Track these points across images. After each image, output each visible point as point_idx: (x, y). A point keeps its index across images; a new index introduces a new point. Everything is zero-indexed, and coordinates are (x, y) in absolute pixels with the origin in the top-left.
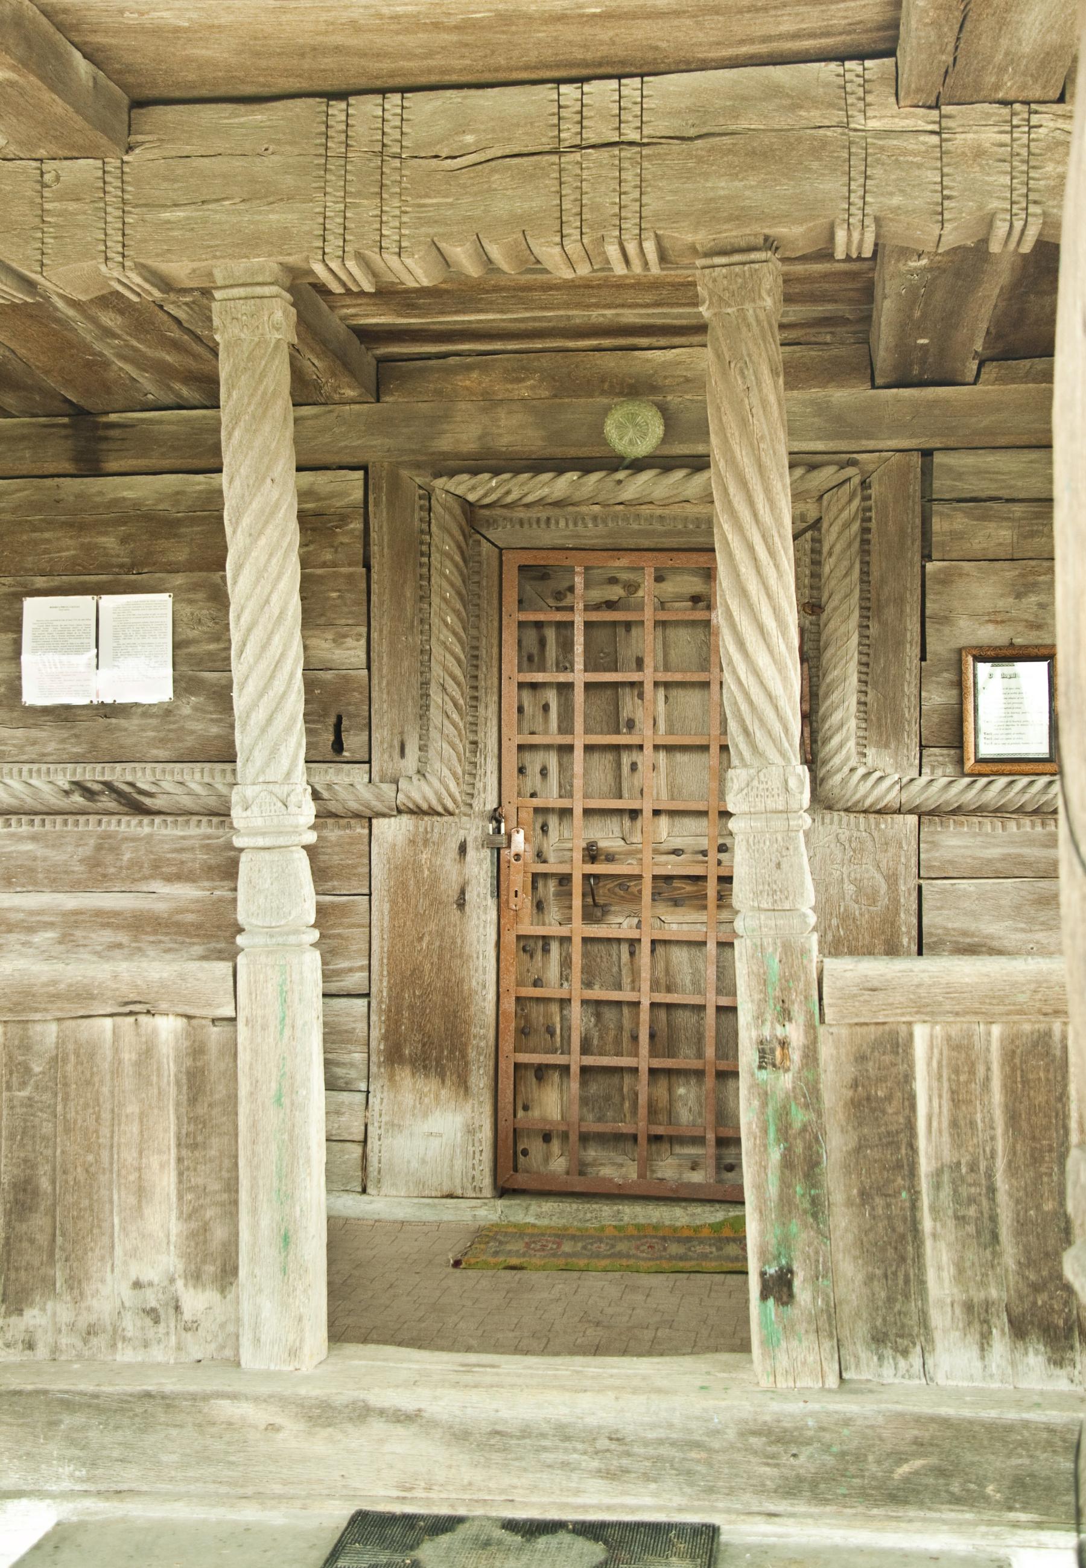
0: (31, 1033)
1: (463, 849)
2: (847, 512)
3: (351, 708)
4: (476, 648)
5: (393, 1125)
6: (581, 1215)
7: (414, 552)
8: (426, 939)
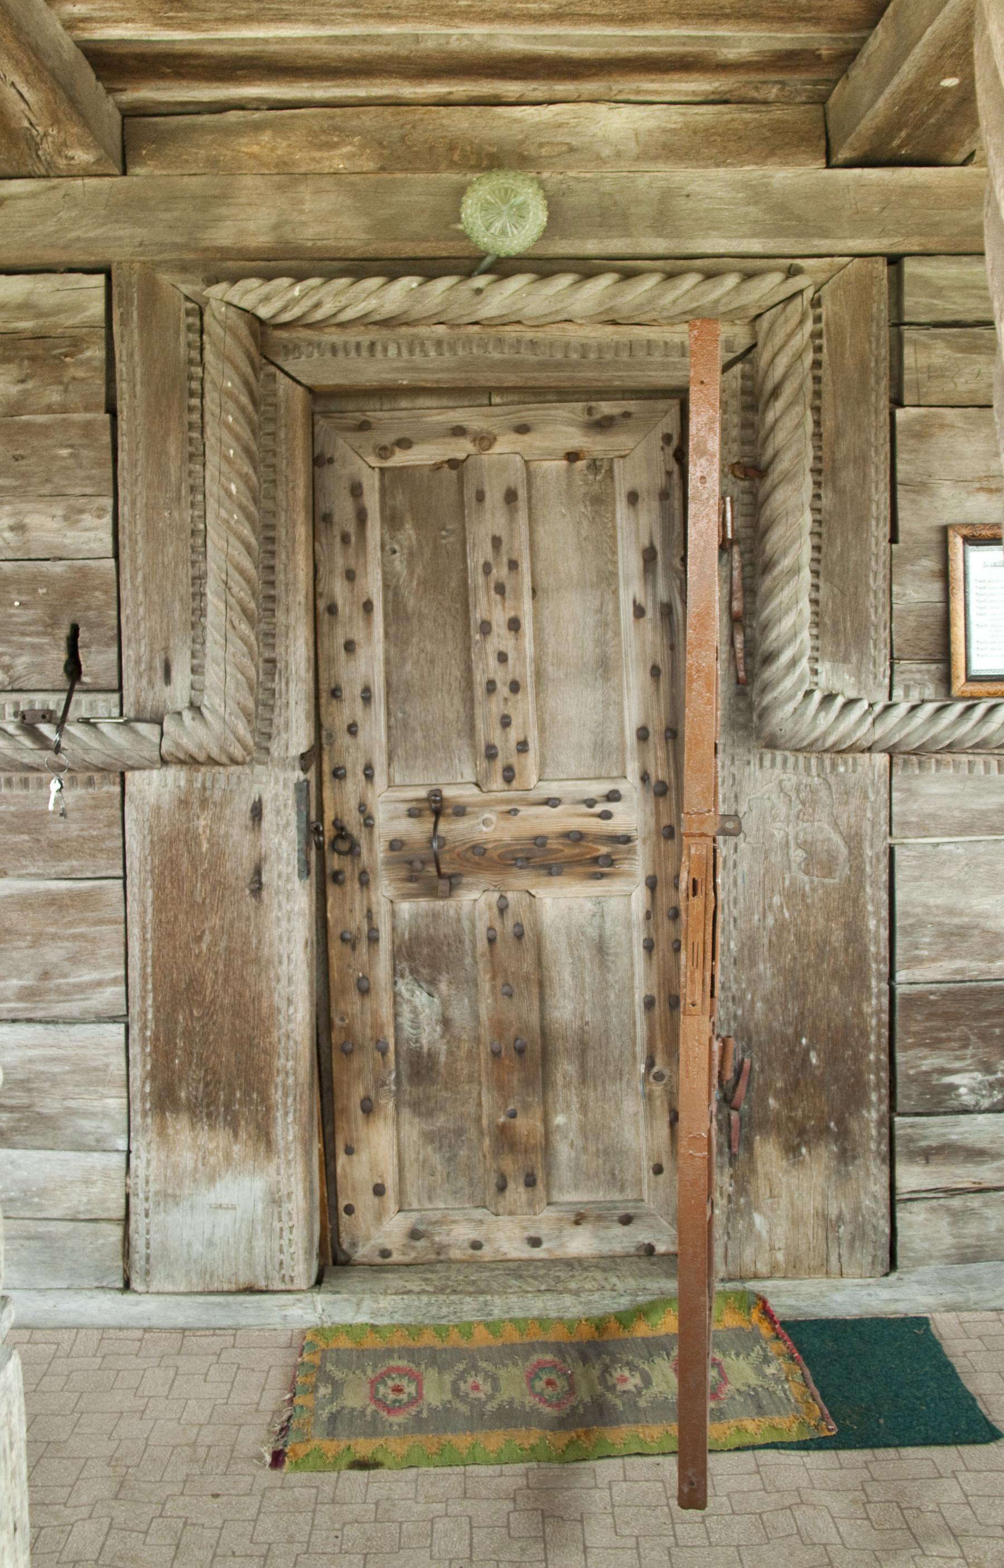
1: (257, 812)
2: (798, 337)
3: (91, 614)
4: (271, 527)
5: (166, 1196)
6: (434, 1310)
7: (180, 390)
8: (207, 938)
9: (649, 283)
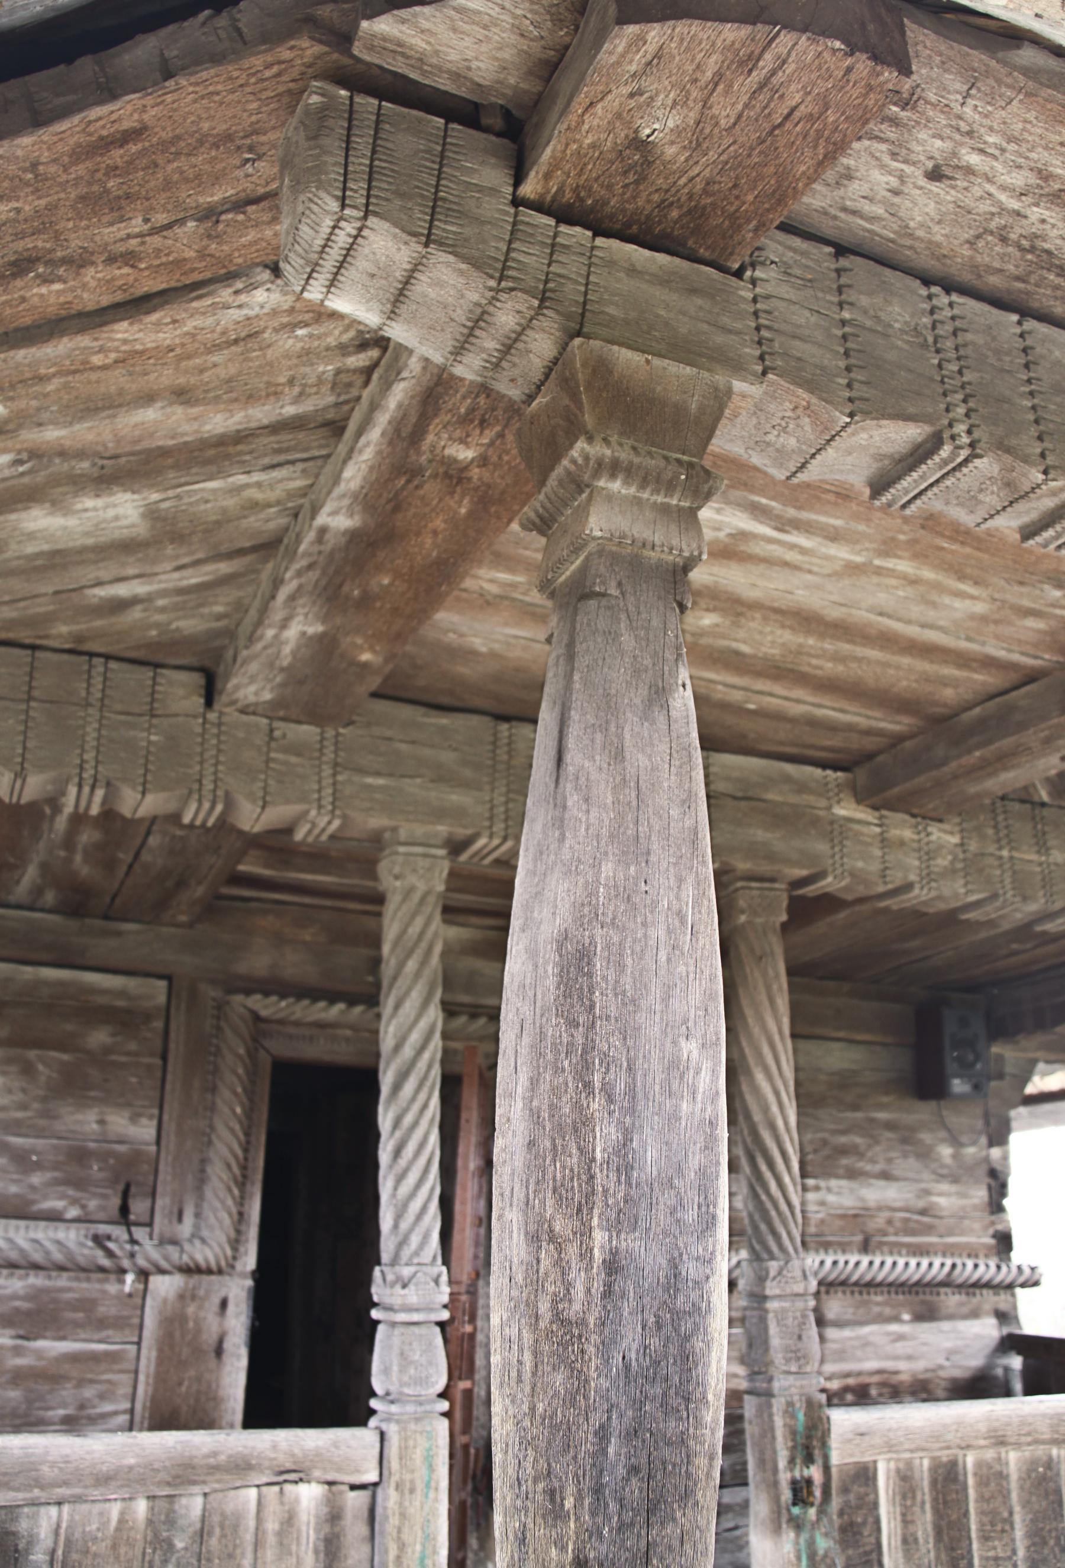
0: (176, 1507)
1: (224, 1304)
9: (463, 1019)
